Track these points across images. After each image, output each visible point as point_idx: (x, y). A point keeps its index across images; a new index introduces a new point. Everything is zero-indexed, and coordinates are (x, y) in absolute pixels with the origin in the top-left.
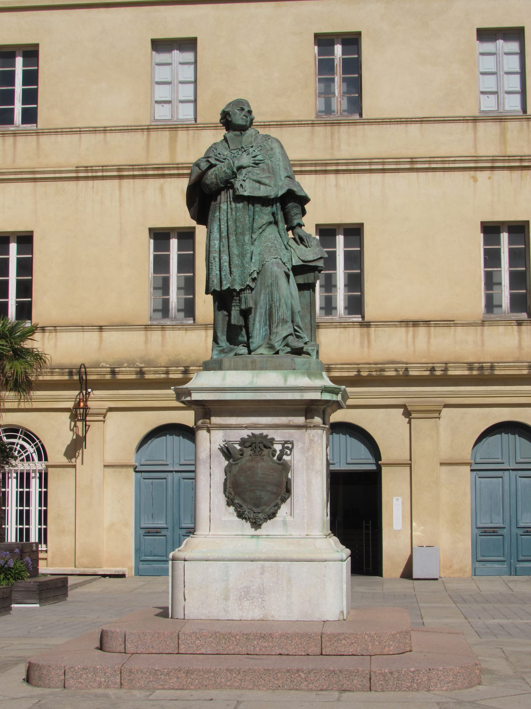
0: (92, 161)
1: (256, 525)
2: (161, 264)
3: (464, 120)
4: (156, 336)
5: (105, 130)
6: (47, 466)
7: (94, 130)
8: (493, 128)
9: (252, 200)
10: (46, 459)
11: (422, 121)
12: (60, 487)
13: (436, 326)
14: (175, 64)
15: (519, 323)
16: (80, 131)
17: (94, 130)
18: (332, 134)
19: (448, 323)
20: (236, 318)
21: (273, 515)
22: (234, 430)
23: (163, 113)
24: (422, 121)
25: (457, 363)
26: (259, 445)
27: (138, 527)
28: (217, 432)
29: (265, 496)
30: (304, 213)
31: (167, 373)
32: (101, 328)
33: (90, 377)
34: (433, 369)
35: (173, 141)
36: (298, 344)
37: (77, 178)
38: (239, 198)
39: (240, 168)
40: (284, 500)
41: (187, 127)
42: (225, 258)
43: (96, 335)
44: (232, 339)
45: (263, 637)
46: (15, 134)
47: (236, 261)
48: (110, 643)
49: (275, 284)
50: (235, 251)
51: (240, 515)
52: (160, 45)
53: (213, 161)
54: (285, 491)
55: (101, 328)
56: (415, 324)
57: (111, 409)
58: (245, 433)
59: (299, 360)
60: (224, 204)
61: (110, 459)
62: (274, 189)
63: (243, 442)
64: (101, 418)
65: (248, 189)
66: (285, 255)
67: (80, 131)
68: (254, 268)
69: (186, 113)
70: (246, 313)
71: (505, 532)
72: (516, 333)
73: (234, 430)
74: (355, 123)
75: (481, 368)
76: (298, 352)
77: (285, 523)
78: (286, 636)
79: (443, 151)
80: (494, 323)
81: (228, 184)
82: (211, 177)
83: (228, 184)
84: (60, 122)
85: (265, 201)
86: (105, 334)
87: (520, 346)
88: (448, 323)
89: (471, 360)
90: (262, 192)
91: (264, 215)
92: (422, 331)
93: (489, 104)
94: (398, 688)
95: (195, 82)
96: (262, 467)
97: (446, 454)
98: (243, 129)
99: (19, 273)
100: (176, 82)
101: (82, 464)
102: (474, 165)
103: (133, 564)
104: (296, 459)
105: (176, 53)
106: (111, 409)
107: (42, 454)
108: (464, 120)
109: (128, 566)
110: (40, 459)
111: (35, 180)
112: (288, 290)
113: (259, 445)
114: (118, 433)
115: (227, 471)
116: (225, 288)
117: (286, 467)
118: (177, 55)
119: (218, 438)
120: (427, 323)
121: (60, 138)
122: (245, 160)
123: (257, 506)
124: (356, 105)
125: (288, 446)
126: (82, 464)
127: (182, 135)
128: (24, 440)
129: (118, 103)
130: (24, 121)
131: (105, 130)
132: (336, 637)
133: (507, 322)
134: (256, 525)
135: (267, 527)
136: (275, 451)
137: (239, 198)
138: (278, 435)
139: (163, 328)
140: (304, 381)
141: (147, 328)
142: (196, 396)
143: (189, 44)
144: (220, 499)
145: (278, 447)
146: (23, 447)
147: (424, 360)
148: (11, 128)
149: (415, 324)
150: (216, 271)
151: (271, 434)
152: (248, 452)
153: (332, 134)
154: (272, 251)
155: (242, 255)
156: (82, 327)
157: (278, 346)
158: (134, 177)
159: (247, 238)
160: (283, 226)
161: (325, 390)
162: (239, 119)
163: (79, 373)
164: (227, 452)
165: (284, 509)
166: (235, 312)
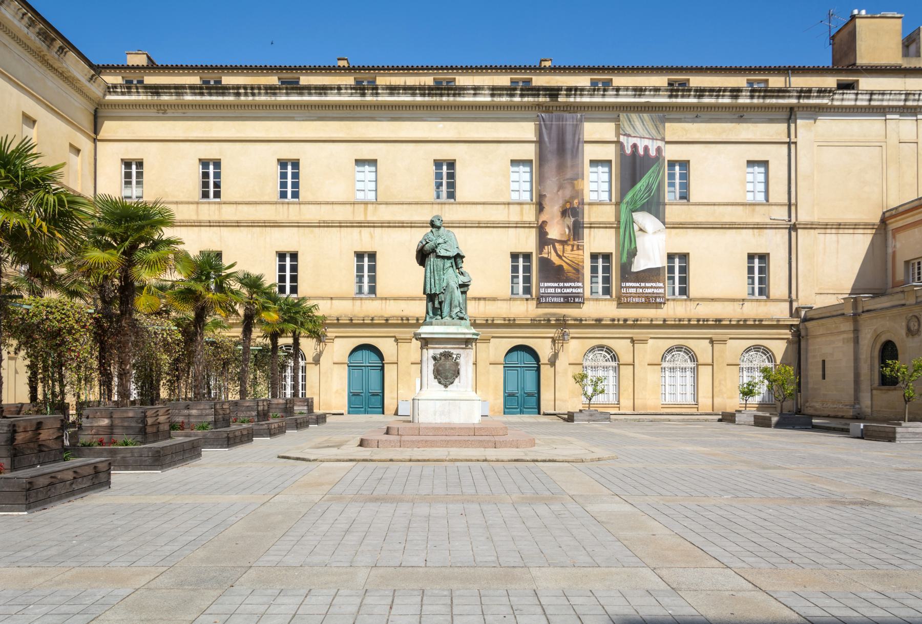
0: (326, 218)
1: (446, 386)
2: (360, 269)
3: (504, 204)
4: (358, 303)
5: (333, 203)
7: (327, 203)
8: (517, 207)
9: (443, 257)
11: (484, 204)
12: (312, 372)
14: (367, 172)
15: (527, 300)
16: (320, 203)
17: (327, 203)
19: (494, 299)
20: (437, 305)
21: (452, 383)
22: (438, 350)
23: (360, 196)
24: (484, 204)
25: (499, 318)
26: (447, 355)
27: (350, 392)
29: (450, 375)
32: (332, 299)
35: (366, 210)
36: (461, 315)
37: (319, 227)
38: (438, 257)
41: (373, 203)
43: (329, 301)
44: (435, 314)
45: (452, 429)
47: (437, 282)
48: (391, 431)
49: (452, 292)
50: (437, 278)
51: (440, 383)
52: (359, 162)
54: (457, 373)
55: (332, 299)
56: (479, 299)
57: (336, 337)
58: (442, 351)
59: (463, 322)
60: (432, 259)
61: (336, 360)
62: (452, 253)
63: (441, 354)
66: (456, 279)
67: (320, 203)
68: (444, 285)
69: (371, 196)
70: (440, 303)
73: (438, 350)
74: (452, 204)
76: (462, 319)
78: (461, 428)
79: (493, 219)
80: (515, 299)
81: (433, 251)
82: (427, 247)
83: (433, 251)
84: (311, 199)
85: (448, 258)
86: (334, 301)
87: (527, 311)
88: (494, 299)
90: (448, 254)
91: (448, 263)
92: (482, 302)
93: (515, 197)
94: (506, 447)
95: (376, 181)
96: (448, 364)
97: (492, 360)
98: (439, 228)
100: (367, 181)
101: (824, 361)
102: (506, 225)
103: (347, 409)
104: (462, 361)
105: (367, 167)
106: (336, 337)
108: (504, 204)
109: (345, 410)
111: (298, 226)
112: (458, 293)
113: (447, 355)
114: (339, 348)
117: (457, 364)
118: (367, 168)
119: (431, 352)
120: (485, 299)
121: (311, 206)
122: (440, 241)
124: (451, 195)
125: (458, 356)
126: (824, 361)
127: (370, 206)
129: (338, 192)
130: (293, 197)
131: (333, 203)
132: (480, 429)
133: (522, 299)
134: (446, 386)
135: (450, 387)
137: (438, 257)
138: (455, 352)
139: (361, 299)
141: (353, 299)
142: (423, 336)
143: (373, 162)
144: (431, 376)
145: (455, 356)
149: (479, 299)
150: (428, 286)
151: (452, 351)
154: (451, 278)
155: (440, 280)
157: (454, 316)
158: (347, 227)
161: (474, 334)
162: (438, 223)
164: (435, 358)
165: (457, 380)
166: (436, 302)
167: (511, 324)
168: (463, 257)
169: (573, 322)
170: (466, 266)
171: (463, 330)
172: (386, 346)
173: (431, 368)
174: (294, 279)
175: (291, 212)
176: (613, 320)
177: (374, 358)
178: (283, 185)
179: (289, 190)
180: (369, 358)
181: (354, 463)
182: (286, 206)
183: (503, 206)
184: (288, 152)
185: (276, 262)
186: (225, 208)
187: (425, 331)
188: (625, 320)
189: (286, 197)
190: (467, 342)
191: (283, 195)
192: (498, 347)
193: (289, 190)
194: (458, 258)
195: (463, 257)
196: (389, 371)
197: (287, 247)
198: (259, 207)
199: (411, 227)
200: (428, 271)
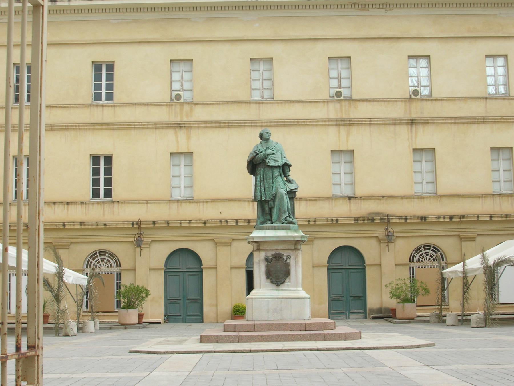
6: (121, 270)
10: (120, 266)
13: (310, 200)
18: (259, 107)
25: (321, 218)
26: (278, 257)
28: (15, 251)
30: (290, 171)
31: (181, 224)
33: (142, 226)
34: (309, 221)
39: (268, 155)
40: (287, 277)
42: (263, 188)
46: (103, 106)
47: (267, 189)
50: (267, 186)
53: (257, 152)
54: (287, 274)
61: (153, 266)
62: (280, 164)
64: (148, 246)
65: (272, 164)
70: (271, 209)
71: (344, 299)
72: (348, 203)
75: (332, 220)
76: (291, 223)
77: (288, 285)
84: (125, 100)
85: (277, 167)
86: (149, 205)
89: (327, 216)
96: (279, 265)
99: (105, 174)
107: (118, 263)
110: (117, 266)
112: (286, 199)
113: (278, 257)
115: (267, 266)
116: (263, 199)
117: (288, 265)
119: (263, 254)
122: (269, 151)
123: (278, 279)
125: (289, 257)
128: (108, 257)
136: (284, 259)
138: (285, 254)
140: (290, 234)
144: (263, 277)
145: (285, 258)
146: (109, 261)
147: (304, 217)
148: (100, 102)
151: (282, 252)
152: (274, 259)
153: (259, 107)
156: (138, 202)
159: (271, 181)
160: (283, 176)
163: (137, 224)
164: (266, 260)
165: (287, 280)
167: (335, 222)
168: (290, 166)
169: (398, 221)
170: (292, 174)
171: (297, 234)
172: (205, 251)
173: (263, 268)
174: (108, 182)
175: (107, 115)
176: (439, 217)
177: (191, 263)
178: (98, 87)
179: (104, 92)
180: (183, 264)
181: (202, 354)
182: (100, 109)
183: (321, 104)
184: (102, 54)
185: (89, 168)
186: (119, 110)
187: (257, 234)
188: (451, 218)
189: (101, 100)
190: (296, 244)
191: (97, 97)
192: (324, 249)
193: (104, 92)
194: (285, 168)
195: (290, 166)
196: (208, 278)
197: (102, 150)
198: (72, 110)
199: (229, 127)
200: (258, 179)
